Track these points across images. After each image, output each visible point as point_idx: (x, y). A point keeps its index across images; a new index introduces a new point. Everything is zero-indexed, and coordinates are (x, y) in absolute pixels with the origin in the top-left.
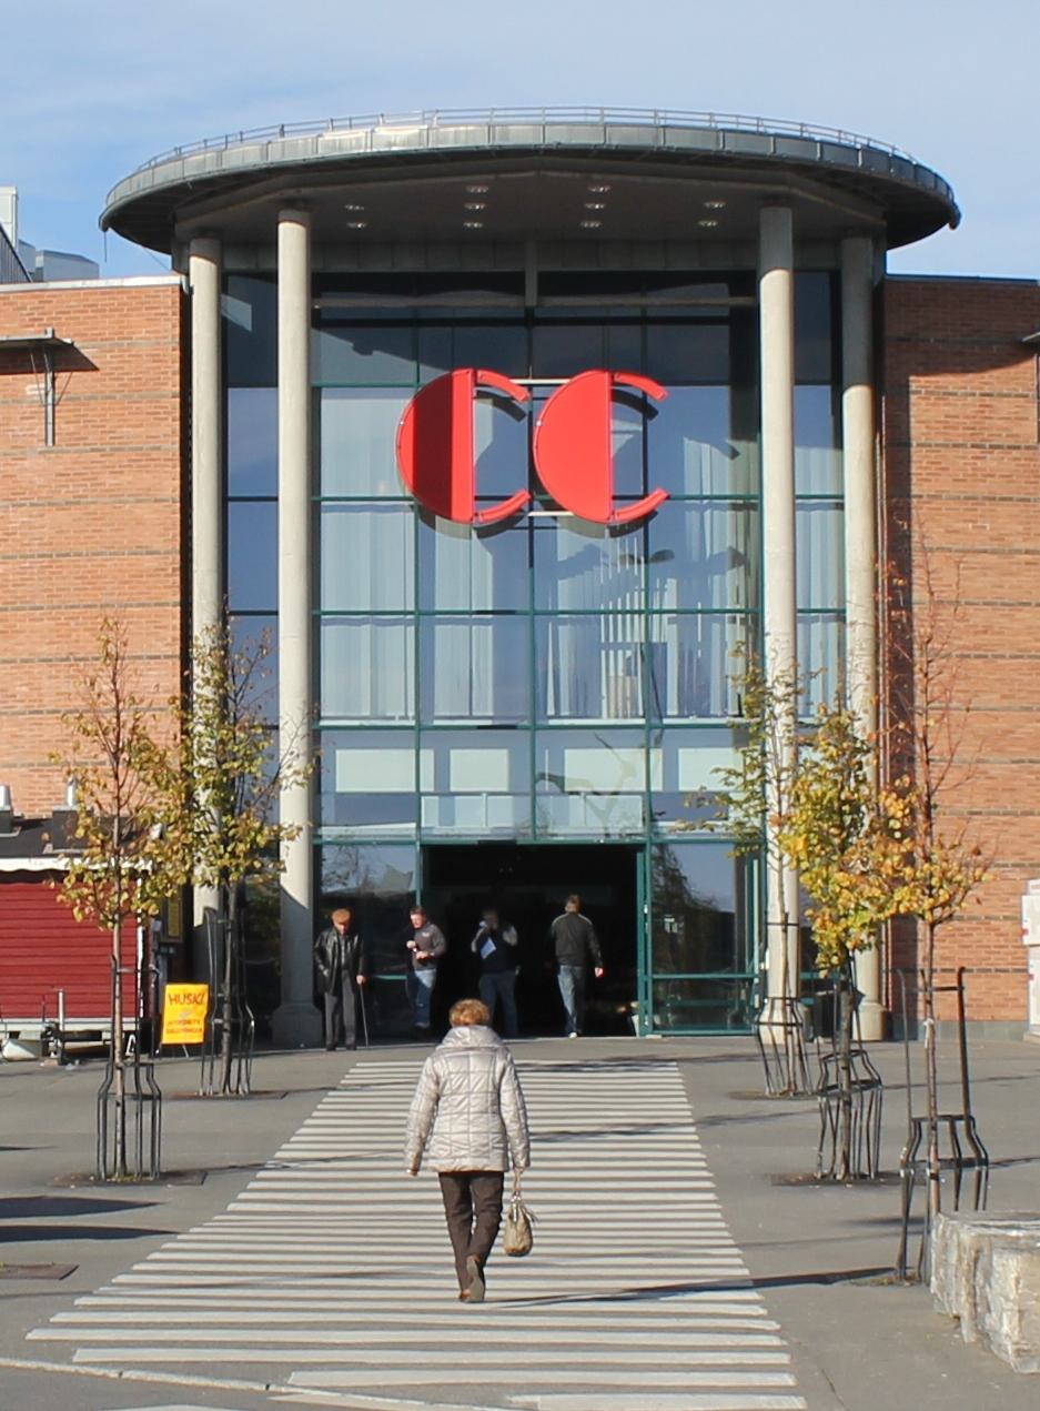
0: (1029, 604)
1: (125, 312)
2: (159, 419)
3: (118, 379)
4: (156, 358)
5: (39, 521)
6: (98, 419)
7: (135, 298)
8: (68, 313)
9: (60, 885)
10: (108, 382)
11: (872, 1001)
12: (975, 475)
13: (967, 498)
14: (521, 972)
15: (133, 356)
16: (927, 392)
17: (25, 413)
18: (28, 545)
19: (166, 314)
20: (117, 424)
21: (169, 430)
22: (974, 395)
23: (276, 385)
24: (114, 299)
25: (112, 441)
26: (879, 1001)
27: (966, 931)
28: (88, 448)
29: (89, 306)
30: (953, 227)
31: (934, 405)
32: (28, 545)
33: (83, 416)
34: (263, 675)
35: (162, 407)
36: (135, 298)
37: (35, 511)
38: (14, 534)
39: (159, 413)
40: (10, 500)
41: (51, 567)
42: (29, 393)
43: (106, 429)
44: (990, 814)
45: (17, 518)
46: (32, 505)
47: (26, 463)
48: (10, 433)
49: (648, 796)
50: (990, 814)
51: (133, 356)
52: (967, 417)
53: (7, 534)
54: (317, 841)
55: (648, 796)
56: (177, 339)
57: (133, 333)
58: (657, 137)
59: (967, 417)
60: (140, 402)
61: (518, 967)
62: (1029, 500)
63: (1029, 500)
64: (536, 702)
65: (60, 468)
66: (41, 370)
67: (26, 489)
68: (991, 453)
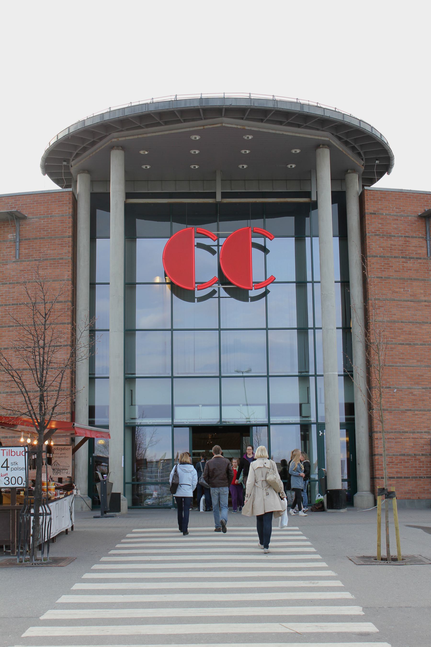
0: (427, 323)
3: (46, 231)
6: (38, 247)
8: (27, 204)
10: (42, 232)
22: (402, 237)
27: (406, 461)
29: (35, 201)
32: (8, 300)
37: (11, 286)
39: (63, 244)
41: (17, 309)
42: (10, 237)
46: (10, 283)
52: (400, 246)
57: (53, 212)
59: (400, 246)
65: (22, 268)
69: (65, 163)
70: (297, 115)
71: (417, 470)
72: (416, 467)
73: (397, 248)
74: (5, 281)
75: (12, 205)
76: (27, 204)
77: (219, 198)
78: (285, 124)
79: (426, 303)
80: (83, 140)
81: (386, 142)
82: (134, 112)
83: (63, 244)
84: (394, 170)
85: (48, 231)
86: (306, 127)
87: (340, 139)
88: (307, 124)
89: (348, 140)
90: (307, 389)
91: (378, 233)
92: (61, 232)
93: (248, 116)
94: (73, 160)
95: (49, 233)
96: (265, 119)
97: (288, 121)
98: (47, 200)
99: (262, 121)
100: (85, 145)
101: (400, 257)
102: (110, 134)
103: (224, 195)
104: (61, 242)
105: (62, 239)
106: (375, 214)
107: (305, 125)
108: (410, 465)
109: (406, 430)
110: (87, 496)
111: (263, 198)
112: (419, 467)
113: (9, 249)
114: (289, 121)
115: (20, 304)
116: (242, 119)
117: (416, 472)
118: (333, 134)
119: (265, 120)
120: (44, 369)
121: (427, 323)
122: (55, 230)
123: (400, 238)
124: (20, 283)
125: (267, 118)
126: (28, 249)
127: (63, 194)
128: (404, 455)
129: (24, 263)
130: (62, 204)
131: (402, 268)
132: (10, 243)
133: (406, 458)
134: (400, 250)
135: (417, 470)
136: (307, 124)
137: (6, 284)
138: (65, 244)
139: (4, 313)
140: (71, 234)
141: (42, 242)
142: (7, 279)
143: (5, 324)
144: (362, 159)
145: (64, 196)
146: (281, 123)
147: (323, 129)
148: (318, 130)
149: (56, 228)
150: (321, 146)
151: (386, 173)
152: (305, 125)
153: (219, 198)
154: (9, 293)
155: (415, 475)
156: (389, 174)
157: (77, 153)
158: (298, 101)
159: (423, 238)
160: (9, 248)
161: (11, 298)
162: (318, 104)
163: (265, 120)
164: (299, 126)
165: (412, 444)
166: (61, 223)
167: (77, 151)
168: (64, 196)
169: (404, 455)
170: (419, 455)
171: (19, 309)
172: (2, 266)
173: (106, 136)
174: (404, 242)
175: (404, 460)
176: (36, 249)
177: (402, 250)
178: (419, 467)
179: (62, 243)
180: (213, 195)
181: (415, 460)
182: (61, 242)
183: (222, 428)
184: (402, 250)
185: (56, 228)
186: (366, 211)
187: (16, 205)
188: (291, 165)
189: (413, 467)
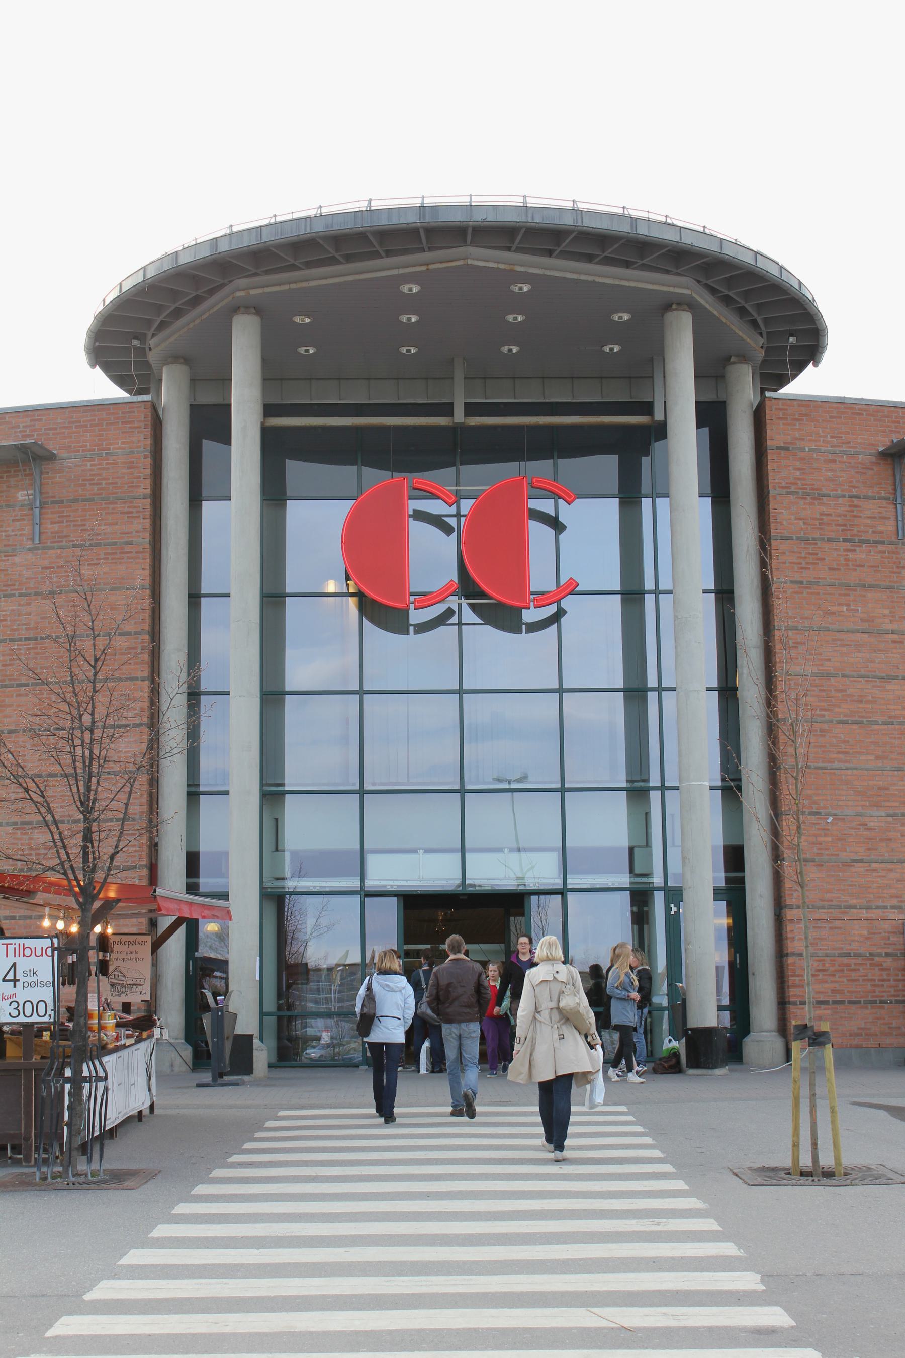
3: (97, 484)
8: (56, 429)
10: (88, 487)
21: (140, 527)
22: (844, 496)
27: (853, 967)
29: (73, 422)
37: (24, 600)
38: (5, 620)
41: (36, 648)
42: (20, 498)
46: (21, 595)
57: (111, 444)
65: (46, 563)
69: (136, 343)
70: (623, 241)
71: (875, 986)
72: (874, 980)
74: (11, 590)
77: (459, 416)
79: (895, 637)
80: (174, 294)
81: (811, 299)
84: (827, 357)
87: (713, 291)
88: (644, 261)
89: (731, 294)
91: (793, 490)
92: (129, 487)
93: (520, 243)
94: (153, 336)
99: (550, 253)
100: (177, 305)
102: (230, 282)
103: (471, 409)
105: (131, 502)
107: (641, 262)
108: (861, 976)
109: (853, 902)
111: (552, 415)
112: (879, 980)
114: (606, 254)
115: (42, 638)
116: (509, 249)
117: (874, 992)
121: (896, 677)
122: (116, 483)
124: (41, 594)
125: (561, 248)
126: (58, 522)
128: (848, 955)
130: (130, 427)
133: (852, 961)
135: (875, 986)
136: (644, 261)
137: (14, 595)
138: (137, 512)
140: (148, 491)
144: (761, 335)
147: (678, 271)
148: (667, 272)
150: (674, 307)
152: (641, 262)
153: (459, 416)
156: (816, 364)
157: (162, 321)
158: (626, 212)
161: (23, 625)
164: (628, 264)
165: (865, 933)
166: (129, 468)
167: (162, 318)
169: (848, 955)
170: (880, 955)
174: (847, 508)
175: (848, 965)
176: (76, 523)
178: (879, 980)
179: (130, 510)
184: (845, 525)
186: (769, 443)
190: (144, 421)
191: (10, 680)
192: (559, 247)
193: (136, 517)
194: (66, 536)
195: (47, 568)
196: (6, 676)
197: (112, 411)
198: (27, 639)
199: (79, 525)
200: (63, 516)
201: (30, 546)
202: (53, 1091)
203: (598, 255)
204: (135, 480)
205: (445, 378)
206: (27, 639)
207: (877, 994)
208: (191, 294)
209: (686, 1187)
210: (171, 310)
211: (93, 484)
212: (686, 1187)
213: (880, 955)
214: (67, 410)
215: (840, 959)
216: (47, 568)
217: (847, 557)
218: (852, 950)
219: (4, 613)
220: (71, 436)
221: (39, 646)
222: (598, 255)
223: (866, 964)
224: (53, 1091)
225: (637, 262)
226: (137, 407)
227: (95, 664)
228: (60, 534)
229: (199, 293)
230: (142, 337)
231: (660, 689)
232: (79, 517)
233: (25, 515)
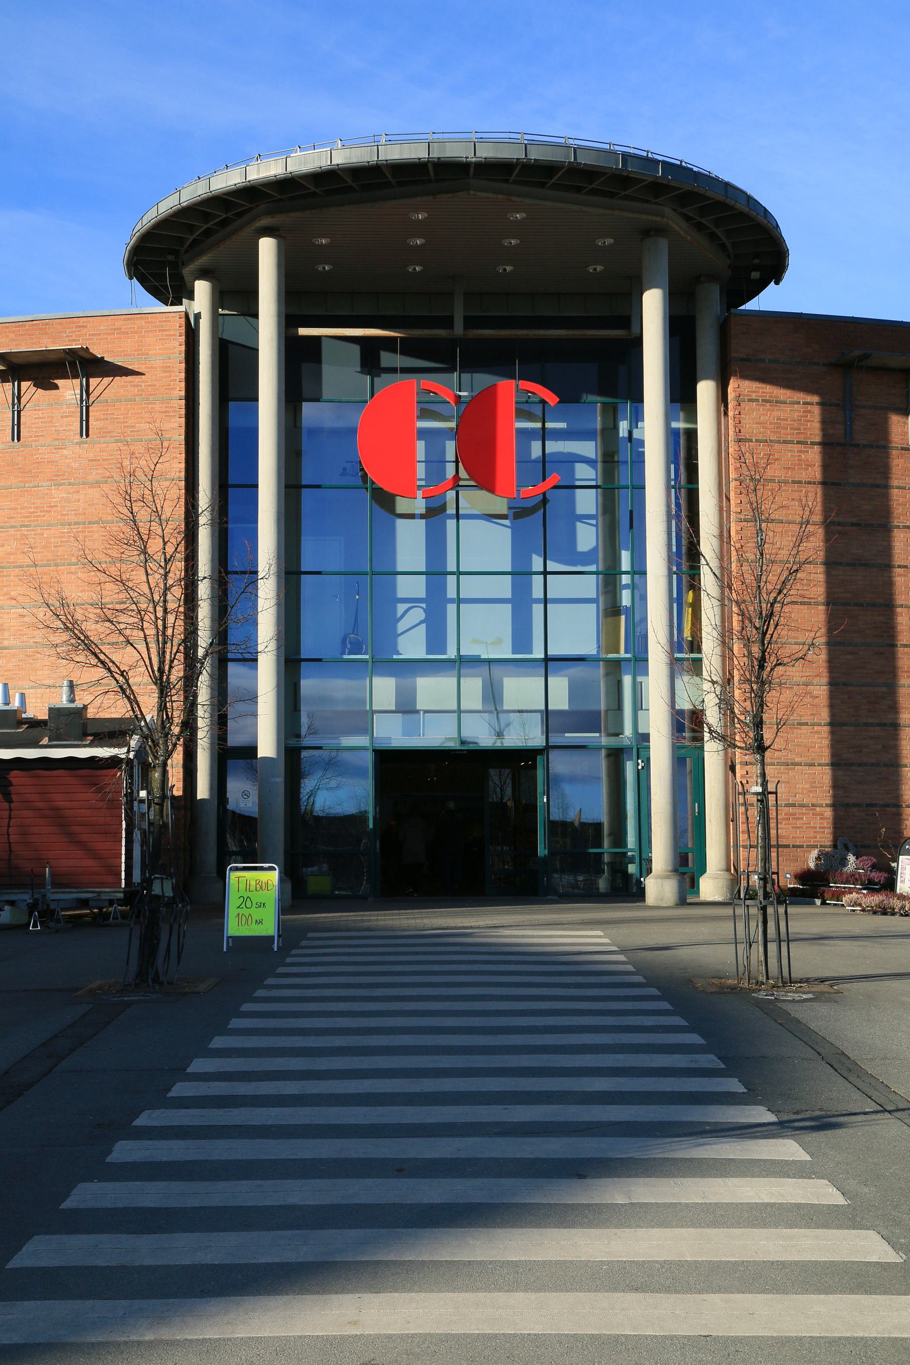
0: (841, 564)
1: (143, 334)
2: (169, 416)
3: (137, 386)
4: (167, 369)
5: (76, 496)
6: (122, 417)
7: (151, 322)
8: (99, 335)
9: (124, 761)
10: (130, 388)
11: (721, 871)
12: (799, 464)
13: (794, 482)
14: (422, 246)
15: (148, 368)
16: (763, 401)
17: (65, 412)
18: (67, 515)
19: (175, 335)
20: (136, 421)
21: (176, 425)
22: (799, 403)
23: (648, 676)
24: (134, 324)
25: (132, 434)
26: (728, 870)
27: (797, 816)
28: (113, 439)
29: (115, 329)
30: (777, 283)
31: (768, 410)
32: (67, 515)
33: (110, 414)
34: (813, 612)
35: (171, 407)
36: (151, 322)
37: (72, 489)
38: (57, 506)
39: (168, 412)
40: (53, 480)
41: (85, 532)
42: (68, 397)
43: (127, 425)
44: (813, 725)
45: (59, 494)
46: (70, 484)
47: (65, 452)
48: (53, 429)
49: (547, 714)
50: (813, 725)
51: (148, 368)
52: (794, 420)
53: (50, 507)
54: (293, 742)
55: (547, 714)
56: (183, 355)
57: (149, 350)
58: (568, 156)
59: (794, 420)
60: (155, 403)
61: (424, 241)
62: (840, 484)
63: (840, 484)
64: (796, 982)
65: (91, 456)
66: (75, 376)
67: (65, 472)
68: (811, 448)
69: (171, 258)
70: (609, 175)
71: (815, 832)
72: (816, 828)
73: (788, 425)
74: (61, 480)
75: (71, 336)
76: (99, 335)
77: (459, 329)
78: (585, 191)
79: (840, 528)
80: (206, 217)
81: (775, 225)
82: (781, 855)
83: (168, 412)
84: (788, 276)
85: (141, 386)
86: (626, 198)
87: (687, 218)
88: (627, 193)
89: (703, 221)
90: (616, 683)
91: (754, 397)
92: (165, 389)
93: (517, 176)
94: (186, 252)
95: (143, 390)
96: (548, 183)
97: (591, 187)
98: (138, 328)
99: (543, 185)
100: (208, 225)
101: (793, 441)
102: (257, 206)
103: (470, 323)
104: (165, 407)
105: (168, 403)
106: (749, 360)
107: (623, 193)
108: (804, 824)
109: (797, 760)
110: (215, 875)
111: (540, 328)
112: (820, 828)
113: (65, 419)
114: (593, 186)
115: (90, 523)
116: (507, 181)
117: (816, 837)
118: (675, 210)
119: (549, 184)
120: (418, 614)
121: (841, 564)
122: (154, 385)
123: (796, 406)
124: (88, 483)
125: (553, 181)
126: (103, 419)
127: (169, 317)
128: (793, 805)
129: (96, 446)
130: (167, 335)
131: (797, 462)
132: (68, 408)
133: (797, 810)
134: (795, 429)
135: (815, 832)
136: (627, 193)
137: (62, 484)
138: (173, 412)
139: (59, 540)
140: (183, 393)
141: (129, 406)
142: (64, 475)
143: (61, 559)
144: (729, 256)
145: (170, 321)
146: (578, 190)
147: (657, 201)
148: (647, 202)
149: (156, 380)
150: (652, 233)
151: (773, 282)
152: (623, 193)
153: (459, 329)
154: (68, 502)
155: (814, 842)
156: (777, 283)
157: (194, 240)
158: (612, 148)
159: (837, 405)
160: (65, 417)
161: (72, 510)
162: (649, 153)
163: (549, 184)
164: (612, 195)
165: (808, 786)
166: (165, 372)
167: (194, 236)
168: (170, 321)
169: (793, 805)
170: (821, 806)
171: (88, 532)
172: (54, 451)
173: (250, 209)
174: (801, 414)
175: (794, 814)
176: (119, 420)
177: (799, 429)
178: (820, 828)
179: (168, 409)
180: (447, 322)
181: (813, 814)
182: (165, 407)
183: (465, 752)
184: (799, 429)
185: (156, 380)
186: (734, 355)
187: (80, 336)
188: (595, 267)
189: (810, 827)
190: (179, 330)
191: (61, 559)
192: (551, 179)
193: (173, 416)
194: (110, 432)
195: (93, 460)
196: (58, 556)
197: (150, 320)
198: (76, 523)
199: (122, 423)
200: (107, 414)
201: (78, 441)
202: (151, 841)
203: (586, 187)
204: (172, 383)
205: (129, 947)
206: (76, 523)
207: (818, 839)
208: (222, 216)
209: (892, 1256)
210: (203, 229)
211: (134, 386)
212: (892, 1256)
213: (821, 806)
214: (109, 318)
215: (787, 809)
216: (93, 460)
217: (800, 458)
218: (796, 801)
219: (55, 500)
220: (114, 342)
221: (87, 530)
222: (586, 187)
223: (808, 814)
224: (151, 841)
225: (620, 193)
226: (172, 317)
227: (166, 564)
228: (104, 430)
229: (228, 215)
230: (176, 253)
231: (459, 601)
232: (121, 415)
233: (73, 412)
